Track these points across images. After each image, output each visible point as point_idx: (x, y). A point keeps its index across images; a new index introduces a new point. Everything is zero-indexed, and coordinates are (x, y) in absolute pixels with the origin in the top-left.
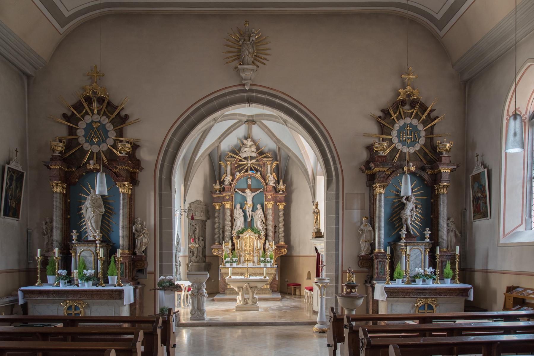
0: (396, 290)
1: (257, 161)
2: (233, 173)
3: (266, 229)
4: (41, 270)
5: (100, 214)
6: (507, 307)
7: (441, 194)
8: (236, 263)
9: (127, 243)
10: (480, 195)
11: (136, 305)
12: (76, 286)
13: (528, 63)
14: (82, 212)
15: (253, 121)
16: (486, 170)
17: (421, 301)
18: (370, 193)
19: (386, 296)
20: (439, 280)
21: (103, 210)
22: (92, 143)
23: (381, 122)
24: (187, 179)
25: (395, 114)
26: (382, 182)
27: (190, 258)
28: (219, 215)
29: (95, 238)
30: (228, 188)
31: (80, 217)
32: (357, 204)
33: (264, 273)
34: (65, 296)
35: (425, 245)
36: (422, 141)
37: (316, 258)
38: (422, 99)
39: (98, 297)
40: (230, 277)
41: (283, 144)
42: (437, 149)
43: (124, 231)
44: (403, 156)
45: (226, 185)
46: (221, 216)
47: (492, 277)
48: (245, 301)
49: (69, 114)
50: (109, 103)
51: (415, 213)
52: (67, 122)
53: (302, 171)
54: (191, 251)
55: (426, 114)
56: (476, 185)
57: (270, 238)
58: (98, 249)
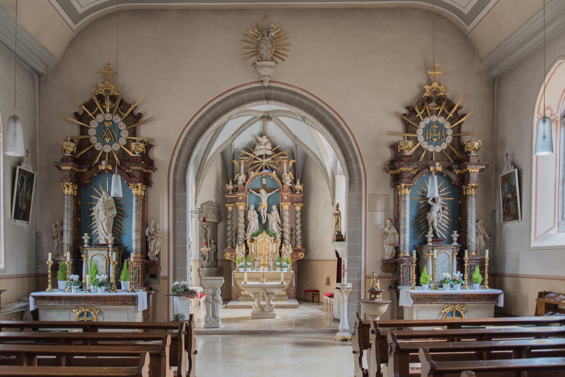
0: (422, 296)
1: (273, 159)
2: (247, 172)
3: (282, 232)
4: (52, 275)
5: (111, 217)
6: (539, 313)
7: (469, 195)
8: (250, 268)
9: (139, 247)
10: (510, 196)
11: (149, 312)
12: (88, 292)
13: (559, 60)
14: (93, 214)
15: (269, 118)
16: (516, 170)
17: (449, 307)
18: (394, 194)
19: (412, 302)
20: (468, 285)
21: (115, 212)
22: (104, 143)
23: (406, 120)
24: (198, 179)
25: (420, 111)
26: (408, 183)
27: (201, 263)
28: (232, 216)
29: (107, 242)
30: (242, 188)
31: (90, 220)
32: (380, 206)
33: (281, 278)
34: (78, 302)
35: (453, 249)
36: (449, 140)
37: (336, 262)
38: (449, 95)
39: (111, 303)
40: (245, 283)
41: (300, 142)
42: (464, 148)
43: (137, 235)
44: (429, 156)
45: (240, 185)
46: (234, 218)
47: (523, 281)
48: (262, 307)
49: (81, 113)
50: (122, 102)
51: (442, 215)
52: (78, 121)
53: (321, 170)
54: (203, 256)
55: (453, 111)
56: (506, 186)
57: (286, 241)
58: (110, 253)
